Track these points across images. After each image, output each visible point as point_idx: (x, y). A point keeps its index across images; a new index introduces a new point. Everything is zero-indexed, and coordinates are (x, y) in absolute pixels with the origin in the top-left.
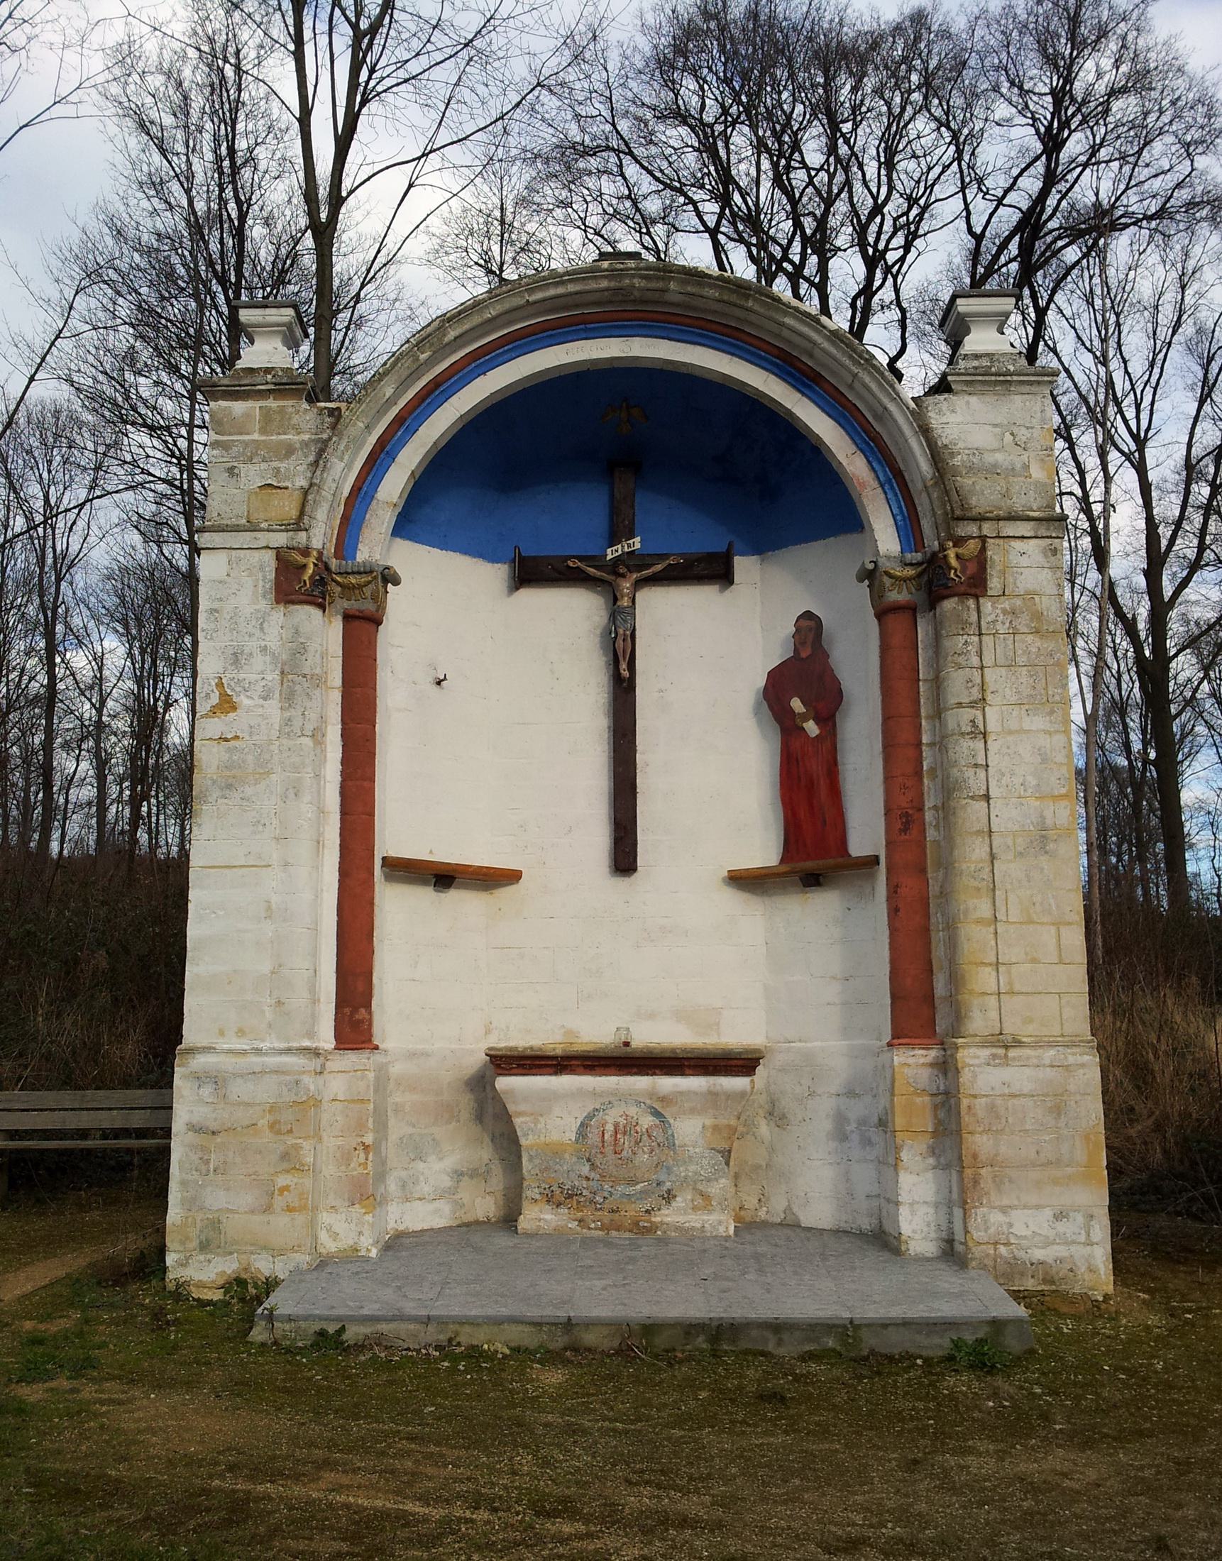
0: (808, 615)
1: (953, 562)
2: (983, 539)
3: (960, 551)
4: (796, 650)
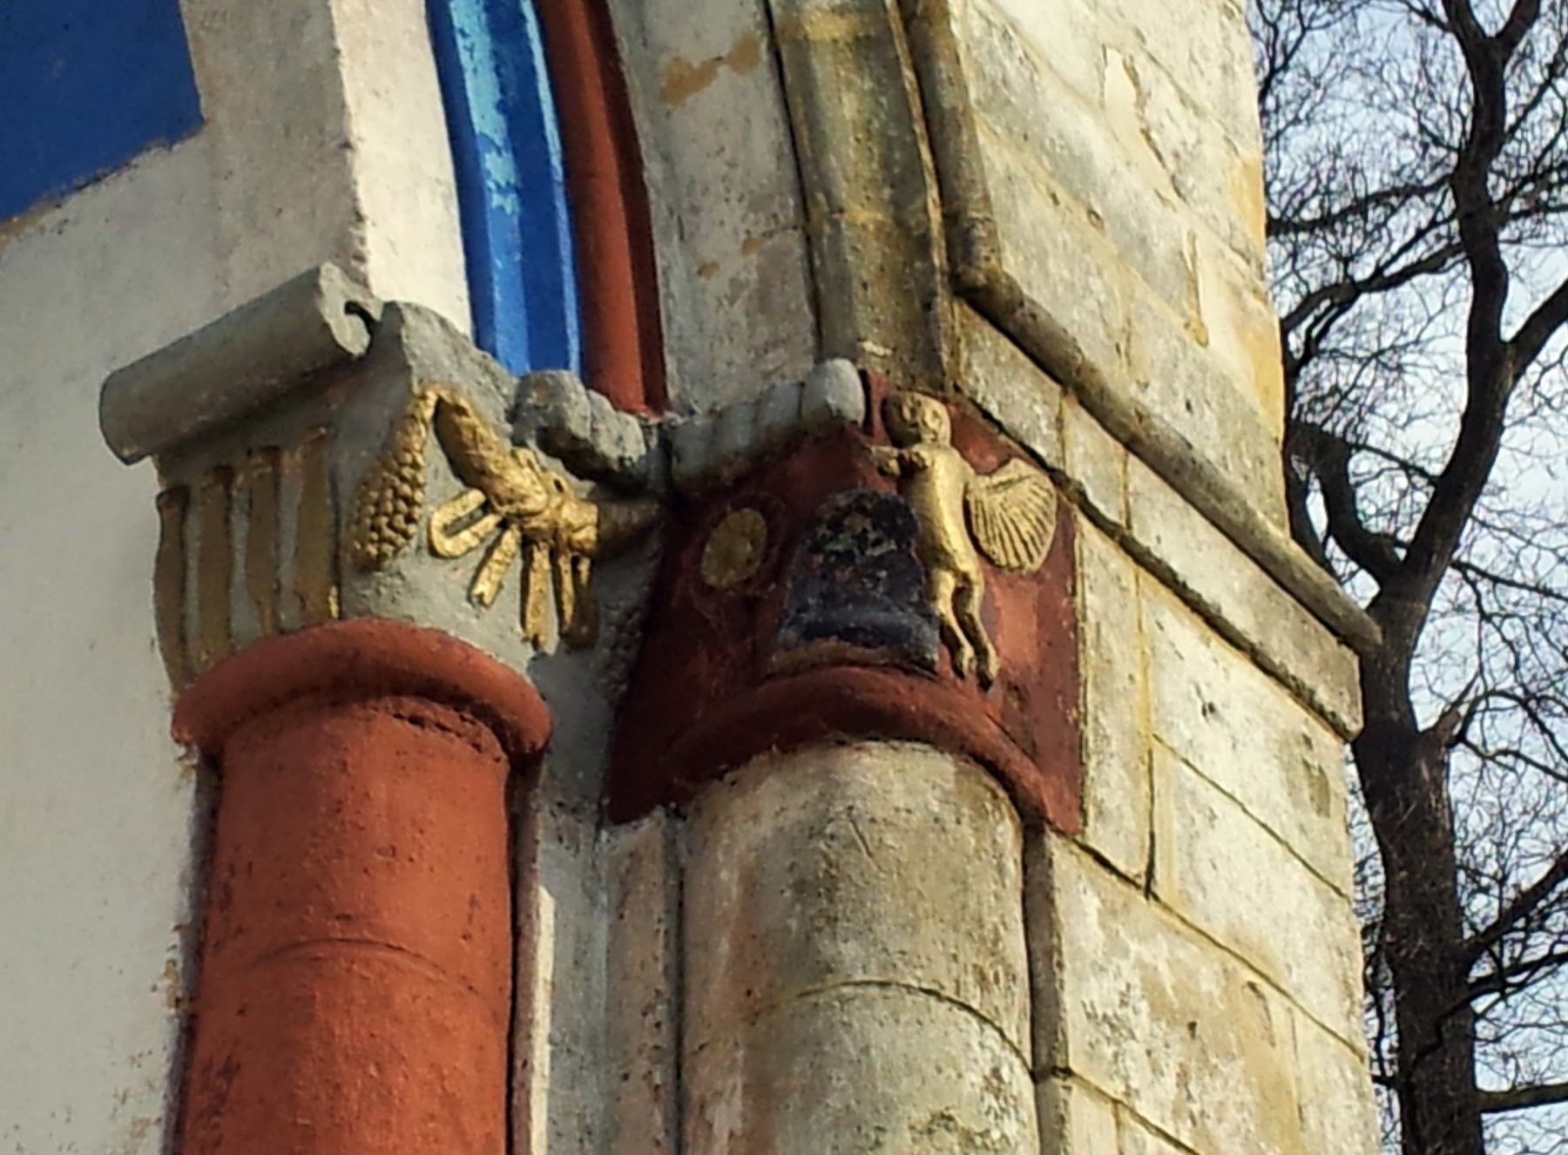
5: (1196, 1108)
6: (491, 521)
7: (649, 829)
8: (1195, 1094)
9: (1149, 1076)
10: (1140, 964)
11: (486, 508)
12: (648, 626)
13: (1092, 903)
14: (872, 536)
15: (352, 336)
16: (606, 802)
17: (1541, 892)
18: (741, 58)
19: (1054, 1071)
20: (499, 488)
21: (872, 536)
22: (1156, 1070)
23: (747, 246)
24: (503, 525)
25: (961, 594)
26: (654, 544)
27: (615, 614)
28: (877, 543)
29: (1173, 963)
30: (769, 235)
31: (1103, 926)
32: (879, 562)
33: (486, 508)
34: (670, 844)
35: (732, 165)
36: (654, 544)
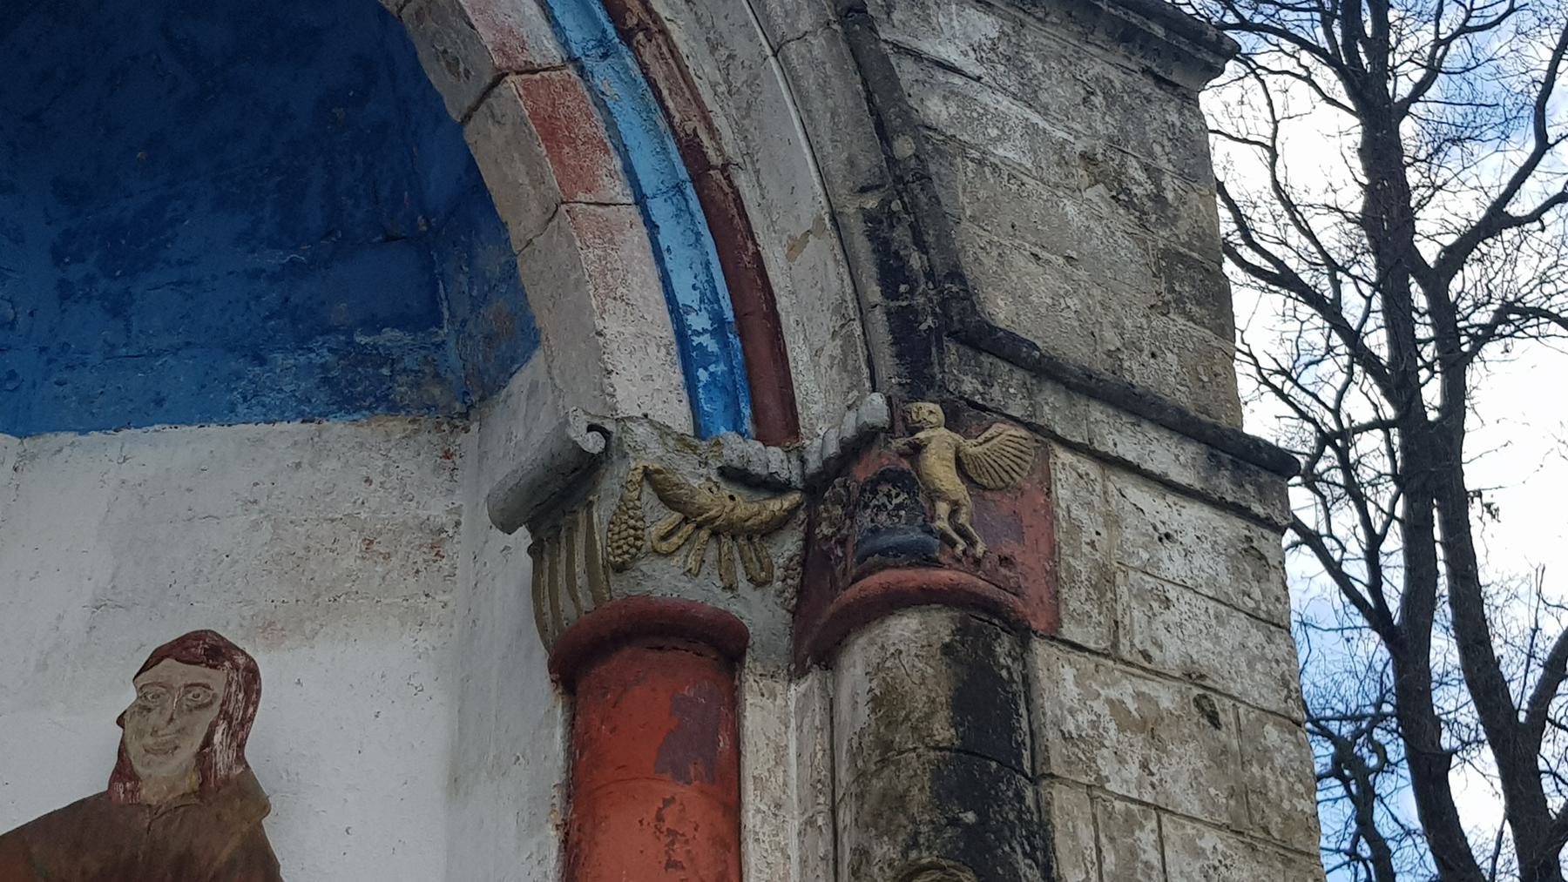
0: (206, 649)
1: (939, 469)
2: (1045, 436)
3: (970, 447)
4: (123, 771)
5: (1155, 779)
6: (689, 528)
7: (812, 680)
8: (1154, 770)
9: (1117, 766)
10: (1110, 702)
11: (686, 520)
12: (804, 563)
13: (1068, 673)
14: (893, 492)
15: (593, 443)
16: (792, 667)
17: (1465, 577)
18: (816, 230)
19: (1044, 776)
20: (690, 508)
21: (893, 492)
22: (1122, 761)
23: (834, 334)
24: (699, 527)
25: (953, 514)
26: (802, 515)
27: (781, 561)
28: (897, 495)
29: (1139, 695)
30: (842, 326)
31: (1077, 684)
32: (899, 507)
33: (686, 520)
34: (824, 688)
35: (822, 290)
36: (802, 515)
